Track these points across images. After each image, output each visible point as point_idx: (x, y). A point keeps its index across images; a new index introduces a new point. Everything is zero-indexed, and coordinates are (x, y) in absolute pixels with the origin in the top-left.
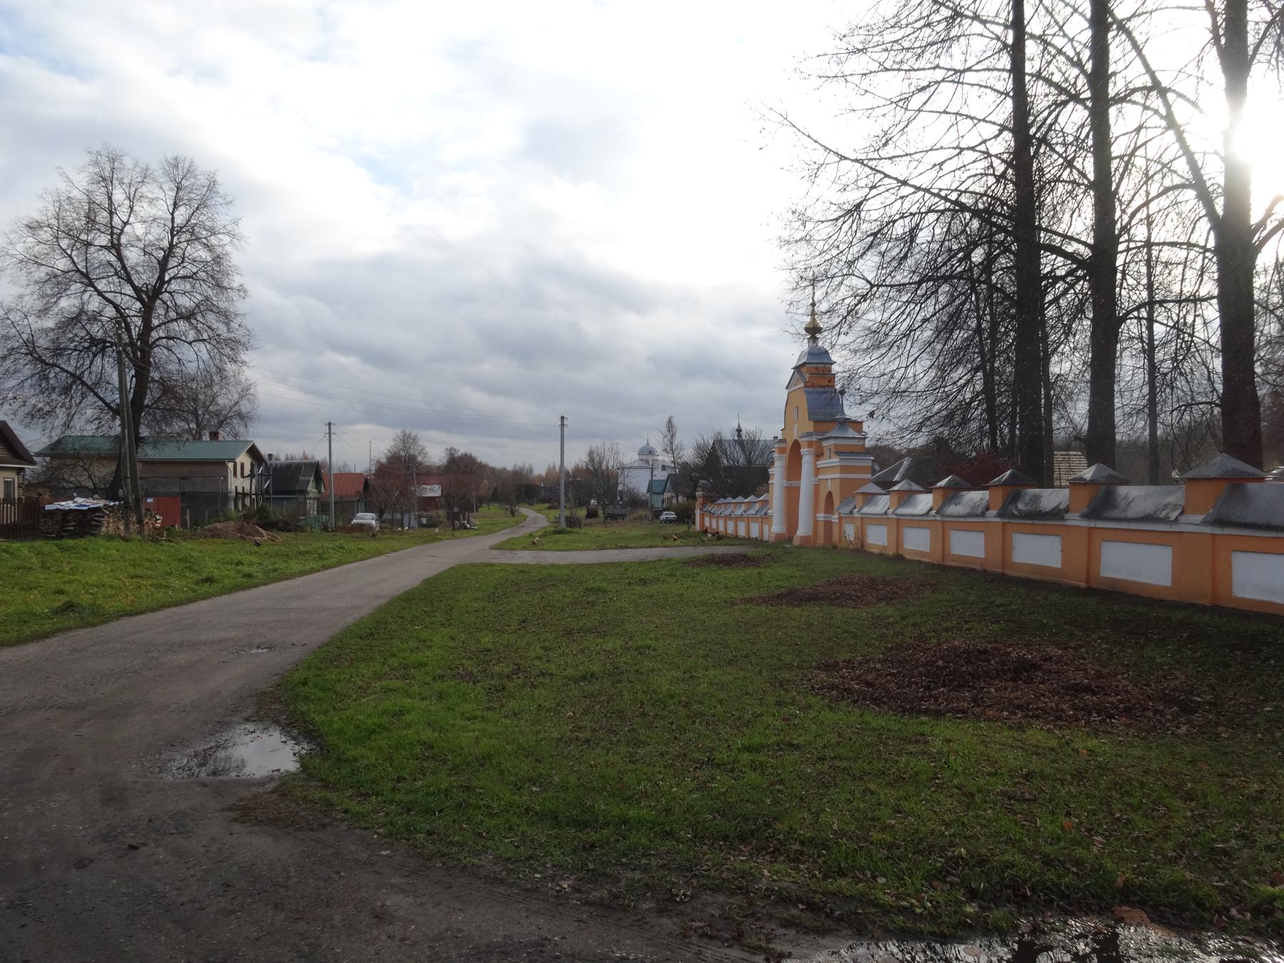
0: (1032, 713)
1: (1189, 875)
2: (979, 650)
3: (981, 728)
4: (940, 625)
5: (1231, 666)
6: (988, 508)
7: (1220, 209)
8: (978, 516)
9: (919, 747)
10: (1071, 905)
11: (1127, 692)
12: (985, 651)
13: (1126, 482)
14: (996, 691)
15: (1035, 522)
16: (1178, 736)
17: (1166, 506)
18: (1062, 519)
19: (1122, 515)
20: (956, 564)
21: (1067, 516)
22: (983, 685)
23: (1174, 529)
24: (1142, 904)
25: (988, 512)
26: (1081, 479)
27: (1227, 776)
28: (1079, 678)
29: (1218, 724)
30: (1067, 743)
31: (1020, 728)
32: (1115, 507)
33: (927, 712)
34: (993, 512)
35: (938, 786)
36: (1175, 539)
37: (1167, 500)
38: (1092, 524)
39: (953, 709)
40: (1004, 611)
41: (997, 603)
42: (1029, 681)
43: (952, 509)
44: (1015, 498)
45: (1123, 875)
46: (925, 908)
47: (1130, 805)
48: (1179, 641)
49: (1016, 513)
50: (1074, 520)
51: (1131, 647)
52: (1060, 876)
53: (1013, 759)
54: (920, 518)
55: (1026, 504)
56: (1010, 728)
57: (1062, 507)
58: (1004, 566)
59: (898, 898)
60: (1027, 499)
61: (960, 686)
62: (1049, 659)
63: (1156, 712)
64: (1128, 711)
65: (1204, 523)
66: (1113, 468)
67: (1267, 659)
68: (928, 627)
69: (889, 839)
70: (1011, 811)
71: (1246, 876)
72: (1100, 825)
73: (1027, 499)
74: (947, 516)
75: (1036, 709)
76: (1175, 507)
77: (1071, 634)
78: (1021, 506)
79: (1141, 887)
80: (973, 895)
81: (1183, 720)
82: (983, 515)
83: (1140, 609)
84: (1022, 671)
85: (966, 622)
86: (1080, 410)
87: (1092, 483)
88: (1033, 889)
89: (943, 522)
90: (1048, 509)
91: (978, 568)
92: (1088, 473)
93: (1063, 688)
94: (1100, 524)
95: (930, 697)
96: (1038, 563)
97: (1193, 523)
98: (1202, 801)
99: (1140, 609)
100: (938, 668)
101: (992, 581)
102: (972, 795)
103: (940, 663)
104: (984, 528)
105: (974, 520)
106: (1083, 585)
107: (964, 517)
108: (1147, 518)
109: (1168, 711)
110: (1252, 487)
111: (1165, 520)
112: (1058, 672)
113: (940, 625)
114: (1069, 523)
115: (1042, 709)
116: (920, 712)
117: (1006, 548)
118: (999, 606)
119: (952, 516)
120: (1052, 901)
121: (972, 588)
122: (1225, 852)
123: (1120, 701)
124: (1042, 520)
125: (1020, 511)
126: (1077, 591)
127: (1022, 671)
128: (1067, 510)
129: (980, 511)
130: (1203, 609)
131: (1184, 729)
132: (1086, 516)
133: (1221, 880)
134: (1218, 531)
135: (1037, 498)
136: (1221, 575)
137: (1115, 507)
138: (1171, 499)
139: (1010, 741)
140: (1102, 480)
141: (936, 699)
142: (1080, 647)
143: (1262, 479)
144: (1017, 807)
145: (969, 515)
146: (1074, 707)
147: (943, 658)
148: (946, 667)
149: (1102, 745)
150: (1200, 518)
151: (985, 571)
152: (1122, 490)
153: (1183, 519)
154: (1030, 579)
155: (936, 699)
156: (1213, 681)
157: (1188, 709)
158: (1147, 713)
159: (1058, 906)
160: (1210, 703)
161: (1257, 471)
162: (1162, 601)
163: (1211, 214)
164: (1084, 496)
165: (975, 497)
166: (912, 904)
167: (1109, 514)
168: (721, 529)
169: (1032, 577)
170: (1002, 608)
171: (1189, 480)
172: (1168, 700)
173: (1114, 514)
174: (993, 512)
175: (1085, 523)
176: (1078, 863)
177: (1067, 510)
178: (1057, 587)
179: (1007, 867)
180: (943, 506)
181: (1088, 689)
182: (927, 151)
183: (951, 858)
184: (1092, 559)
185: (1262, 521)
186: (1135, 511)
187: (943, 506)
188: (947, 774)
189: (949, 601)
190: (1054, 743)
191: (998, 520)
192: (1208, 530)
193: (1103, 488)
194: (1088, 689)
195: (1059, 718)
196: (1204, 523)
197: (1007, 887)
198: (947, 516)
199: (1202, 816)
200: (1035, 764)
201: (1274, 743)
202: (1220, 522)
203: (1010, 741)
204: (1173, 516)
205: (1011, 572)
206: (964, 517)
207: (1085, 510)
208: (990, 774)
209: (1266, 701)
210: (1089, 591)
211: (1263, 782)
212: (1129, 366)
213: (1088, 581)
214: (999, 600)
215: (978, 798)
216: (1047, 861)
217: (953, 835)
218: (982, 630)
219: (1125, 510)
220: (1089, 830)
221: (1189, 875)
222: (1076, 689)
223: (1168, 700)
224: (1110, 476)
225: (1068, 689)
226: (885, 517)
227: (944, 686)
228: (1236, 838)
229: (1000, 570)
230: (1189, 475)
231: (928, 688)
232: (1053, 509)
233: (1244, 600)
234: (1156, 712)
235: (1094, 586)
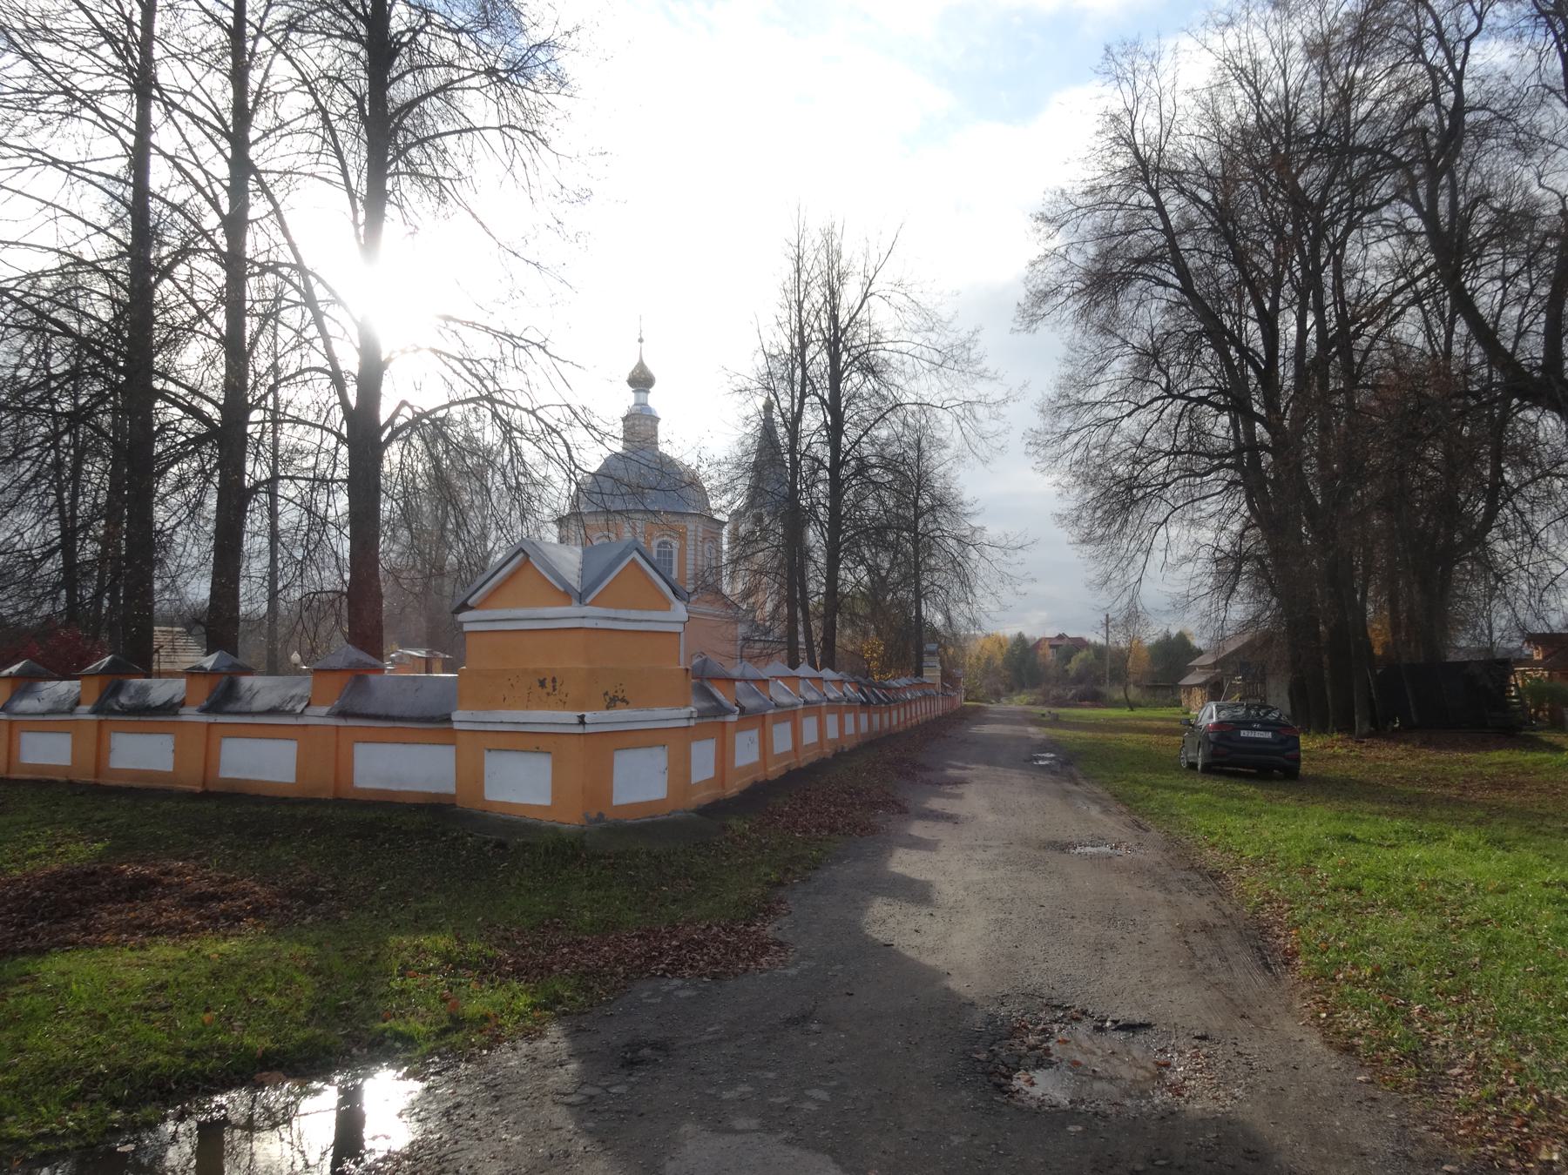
0: (152, 931)
1: (318, 1032)
2: (86, 873)
3: (97, 955)
4: (22, 853)
5: (351, 854)
6: (78, 703)
7: (353, 401)
8: (63, 712)
9: (27, 987)
10: (215, 1085)
11: (255, 893)
12: (93, 873)
13: (249, 672)
14: (110, 914)
15: (143, 718)
16: (304, 926)
17: (292, 698)
18: (176, 714)
19: (246, 708)
20: (28, 776)
21: (183, 710)
22: (93, 910)
23: (301, 721)
24: (279, 1066)
25: (80, 708)
26: (201, 668)
27: (348, 949)
28: (205, 887)
29: (339, 909)
30: (197, 951)
31: (143, 947)
32: (238, 699)
33: (24, 951)
34: (85, 708)
35: (62, 1017)
36: (300, 733)
37: (293, 692)
38: (211, 719)
39: (60, 942)
40: (107, 827)
41: (97, 818)
42: (148, 898)
43: (27, 704)
44: (117, 689)
45: (262, 1044)
46: (68, 1128)
47: (265, 989)
48: (304, 836)
49: (117, 708)
50: (190, 715)
51: (256, 849)
52: (204, 1064)
53: (140, 976)
54: (40, 718)
55: (131, 698)
56: (132, 949)
57: (176, 700)
58: (97, 773)
59: (33, 1128)
60: (132, 691)
61: (64, 917)
62: (168, 873)
63: (283, 908)
64: (256, 912)
65: (329, 715)
66: (236, 656)
67: (383, 844)
68: (6, 857)
69: (15, 1078)
70: (148, 1021)
71: (364, 1022)
72: (239, 1012)
73: (132, 691)
74: (16, 714)
75: (160, 925)
76: (302, 699)
77: (191, 843)
78: (123, 699)
79: (278, 1051)
80: (116, 1103)
81: (308, 911)
82: (71, 711)
83: (264, 809)
84: (139, 889)
85: (58, 845)
86: (199, 590)
87: (214, 672)
88: (177, 1083)
89: (11, 723)
90: (158, 703)
91: (61, 778)
92: (209, 662)
93: (186, 900)
94: (221, 719)
95: (26, 934)
96: (143, 767)
97: (319, 715)
98: (328, 973)
99: (264, 809)
100: (34, 899)
101: (82, 794)
102: (104, 1016)
103: (37, 894)
104: (73, 728)
105: (57, 718)
106: (199, 789)
107: (44, 714)
108: (273, 711)
109: (295, 905)
110: (373, 677)
111: (291, 713)
112: (180, 885)
113: (22, 853)
114: (184, 718)
115: (166, 924)
116: (15, 954)
117: (101, 751)
118: (99, 822)
119: (24, 713)
120: (196, 1088)
121: (57, 804)
122: (347, 1007)
123: (248, 903)
124: (151, 715)
125: (122, 706)
126: (192, 796)
127: (139, 889)
128: (182, 704)
129: (66, 707)
130: (324, 803)
131: (309, 919)
132: (205, 710)
133: (344, 1029)
134: (341, 722)
135: (145, 690)
136: (344, 766)
137: (238, 699)
138: (298, 691)
139: (135, 960)
140: (224, 669)
141: (34, 936)
142: (201, 855)
143: (382, 670)
144: (154, 1016)
145: (50, 712)
146: (200, 917)
147: (39, 888)
148: (45, 897)
149: (231, 946)
150: (326, 710)
151: (70, 782)
152: (246, 681)
153: (308, 711)
154: (132, 788)
155: (34, 936)
156: (335, 870)
157: (312, 900)
158: (274, 911)
159: (203, 1090)
160: (332, 892)
161: (378, 663)
162: (286, 798)
163: (344, 403)
164: (203, 689)
165: (62, 688)
166: (52, 1129)
167: (231, 707)
168: (864, 718)
169: (135, 784)
170: (105, 824)
171: (316, 670)
172: (291, 894)
173: (237, 707)
174: (85, 708)
175: (204, 719)
176: (221, 1047)
177: (182, 704)
178: (167, 794)
179: (152, 1069)
180: (11, 700)
181: (214, 897)
182: (17, 243)
183: (88, 1078)
184: (210, 758)
185: (381, 712)
186: (260, 703)
187: (11, 700)
188: (70, 1003)
189: (30, 822)
190: (183, 954)
191: (93, 717)
192: (332, 722)
193: (225, 678)
194: (214, 897)
195: (185, 930)
196: (329, 715)
197: (151, 1088)
198: (16, 714)
199: (328, 985)
200: (165, 975)
201: (387, 916)
202: (343, 714)
203: (135, 960)
204: (299, 709)
205: (106, 781)
206: (44, 714)
207: (205, 703)
208: (120, 994)
209: (381, 881)
210: (206, 795)
211: (377, 947)
212: (254, 542)
213: (204, 784)
214: (99, 815)
215: (111, 1017)
216: (191, 1055)
217: (90, 1056)
218: (81, 852)
219: (249, 703)
220: (228, 1019)
221: (318, 1032)
222: (202, 899)
223: (291, 894)
224: (233, 666)
225: (193, 899)
226: (579, 730)
227: (42, 919)
228: (357, 995)
229: (91, 780)
230: (318, 665)
231: (22, 925)
232: (165, 703)
233: (364, 790)
234: (283, 908)
235: (211, 789)
